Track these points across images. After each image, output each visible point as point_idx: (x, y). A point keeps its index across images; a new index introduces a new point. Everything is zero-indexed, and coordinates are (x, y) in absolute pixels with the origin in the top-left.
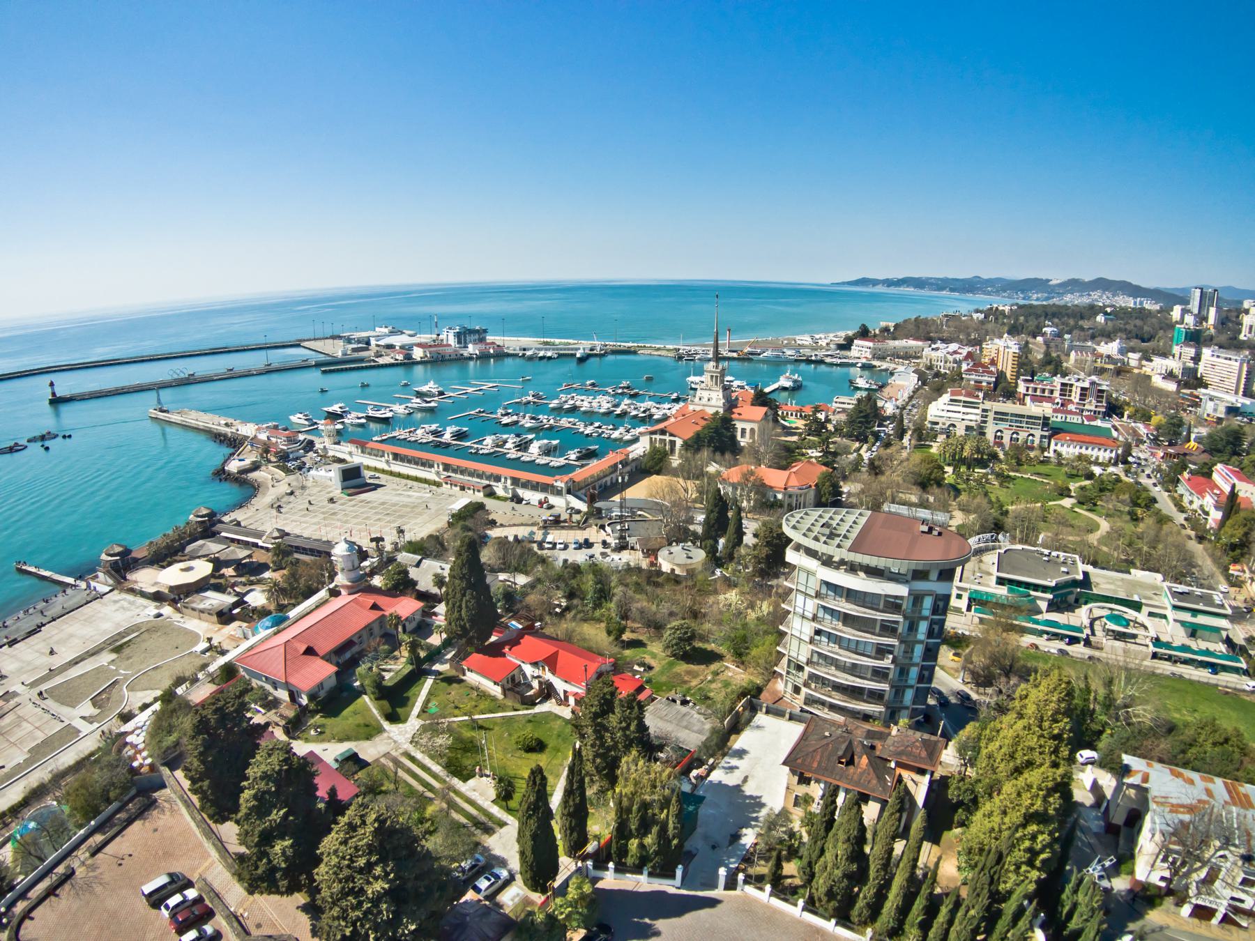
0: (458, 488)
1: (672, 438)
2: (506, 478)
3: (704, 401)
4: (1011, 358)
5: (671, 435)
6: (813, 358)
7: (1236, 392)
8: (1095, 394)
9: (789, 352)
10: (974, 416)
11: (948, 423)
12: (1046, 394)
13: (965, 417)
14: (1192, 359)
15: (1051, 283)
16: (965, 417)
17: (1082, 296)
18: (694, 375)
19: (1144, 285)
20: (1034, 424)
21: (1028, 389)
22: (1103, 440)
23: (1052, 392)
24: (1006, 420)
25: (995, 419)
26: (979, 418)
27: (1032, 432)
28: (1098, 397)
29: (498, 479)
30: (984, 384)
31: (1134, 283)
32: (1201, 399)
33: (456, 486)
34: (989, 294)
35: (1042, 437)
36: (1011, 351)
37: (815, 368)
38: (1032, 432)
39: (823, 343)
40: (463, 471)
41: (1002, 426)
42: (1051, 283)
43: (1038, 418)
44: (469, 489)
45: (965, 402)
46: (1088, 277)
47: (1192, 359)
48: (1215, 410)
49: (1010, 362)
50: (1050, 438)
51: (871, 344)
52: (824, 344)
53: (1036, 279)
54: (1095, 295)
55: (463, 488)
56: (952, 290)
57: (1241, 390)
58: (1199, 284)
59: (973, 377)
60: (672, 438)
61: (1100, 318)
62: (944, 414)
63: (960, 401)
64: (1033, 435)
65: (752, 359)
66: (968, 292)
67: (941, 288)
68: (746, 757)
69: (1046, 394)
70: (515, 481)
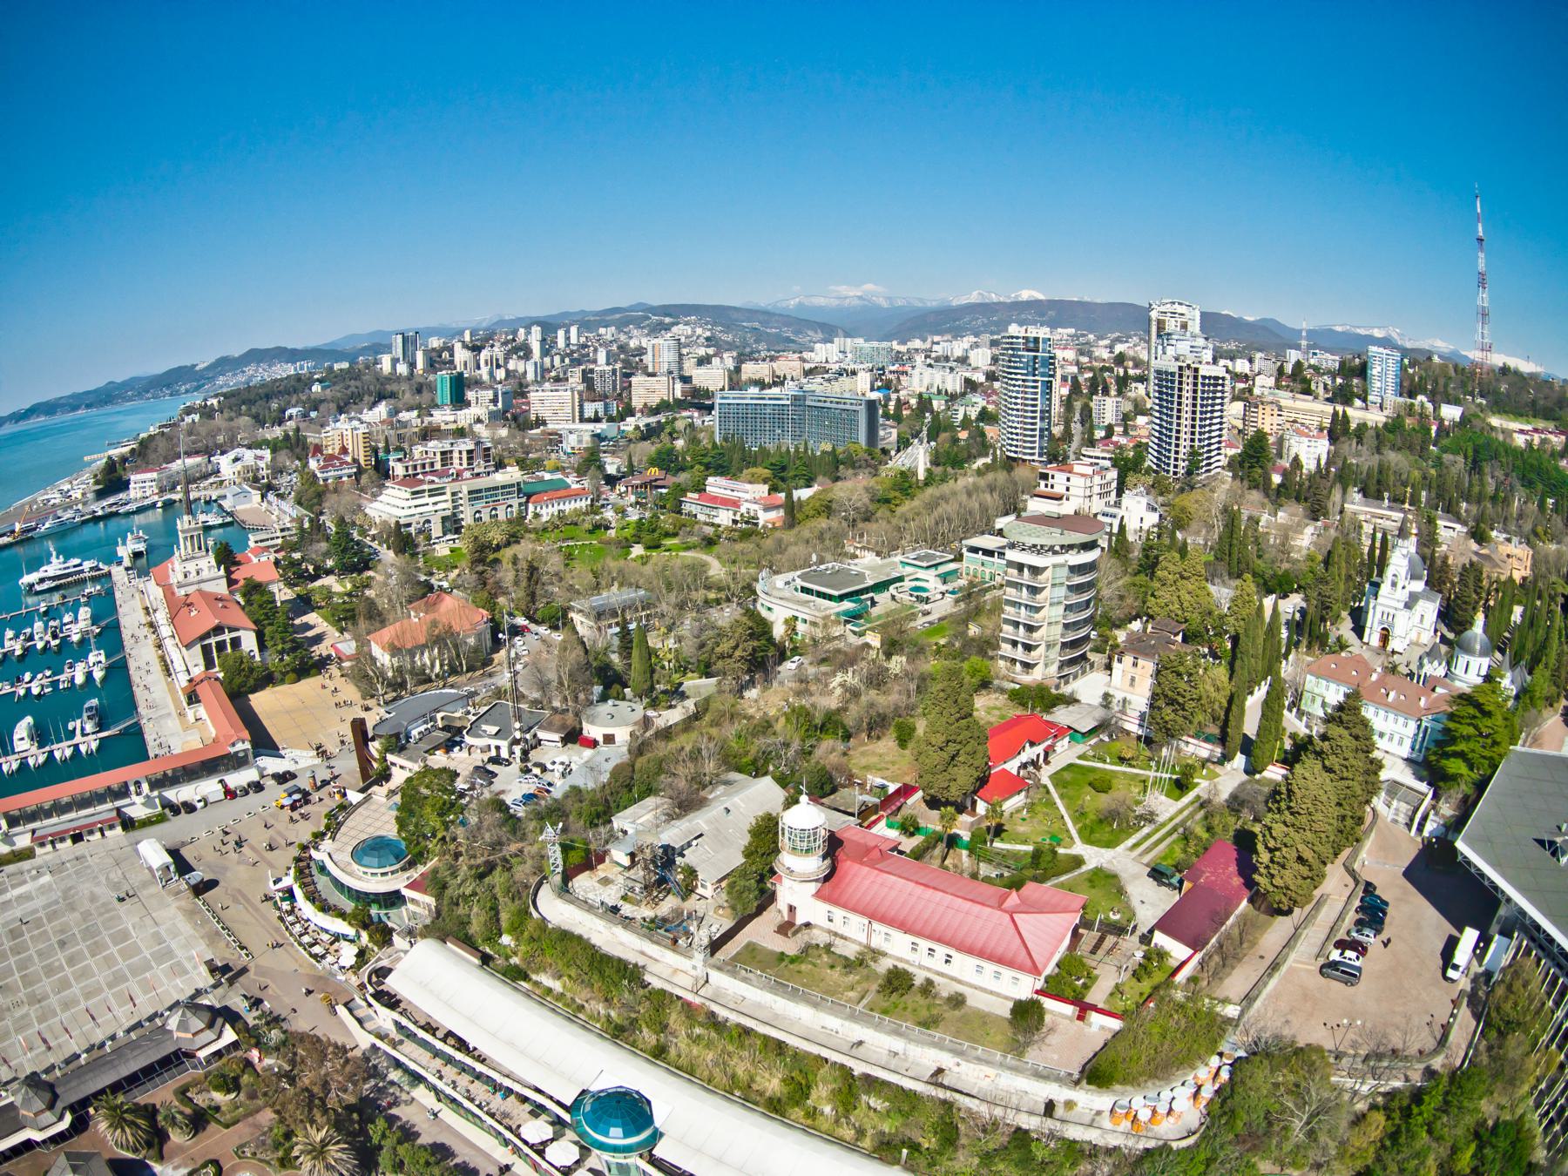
0: (69, 842)
1: (234, 635)
2: (138, 784)
3: (193, 577)
4: (361, 440)
5: (231, 630)
6: (100, 513)
7: (574, 421)
8: (482, 453)
9: (69, 514)
10: (444, 504)
11: (422, 520)
12: (427, 469)
13: (437, 507)
14: (491, 401)
15: (197, 368)
16: (437, 507)
17: (234, 375)
18: (29, 573)
19: (299, 346)
20: (509, 493)
21: (407, 468)
22: (562, 493)
23: (432, 465)
24: (481, 498)
25: (470, 500)
26: (449, 505)
27: (509, 502)
28: (485, 456)
29: (123, 792)
30: (345, 479)
31: (290, 346)
32: (560, 436)
33: (62, 840)
34: (130, 399)
35: (520, 505)
36: (360, 432)
37: (105, 525)
38: (509, 502)
39: (77, 494)
40: (59, 808)
41: (479, 505)
42: (197, 368)
43: (513, 485)
44: (91, 832)
45: (430, 491)
46: (237, 352)
47: (491, 401)
48: (580, 442)
49: (361, 445)
50: (527, 502)
51: (154, 475)
52: (79, 496)
53: (180, 368)
54: (250, 370)
55: (77, 838)
56: (88, 406)
57: (577, 418)
58: (401, 328)
59: (332, 473)
60: (234, 635)
61: (316, 388)
62: (413, 511)
63: (424, 491)
64: (511, 506)
65: (32, 538)
66: (106, 403)
67: (75, 408)
68: (794, 904)
69: (427, 469)
70: (156, 784)
